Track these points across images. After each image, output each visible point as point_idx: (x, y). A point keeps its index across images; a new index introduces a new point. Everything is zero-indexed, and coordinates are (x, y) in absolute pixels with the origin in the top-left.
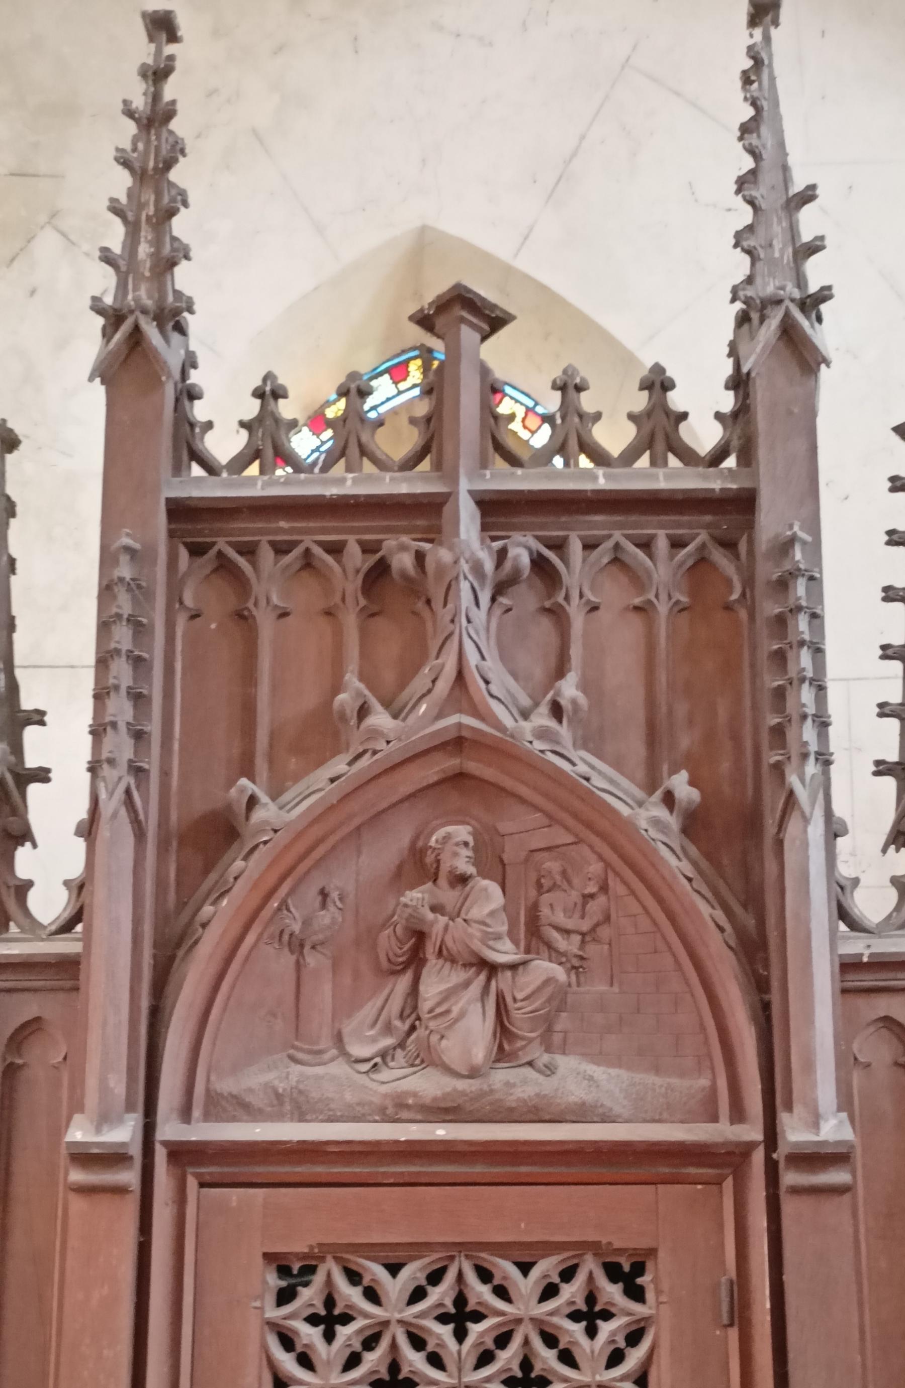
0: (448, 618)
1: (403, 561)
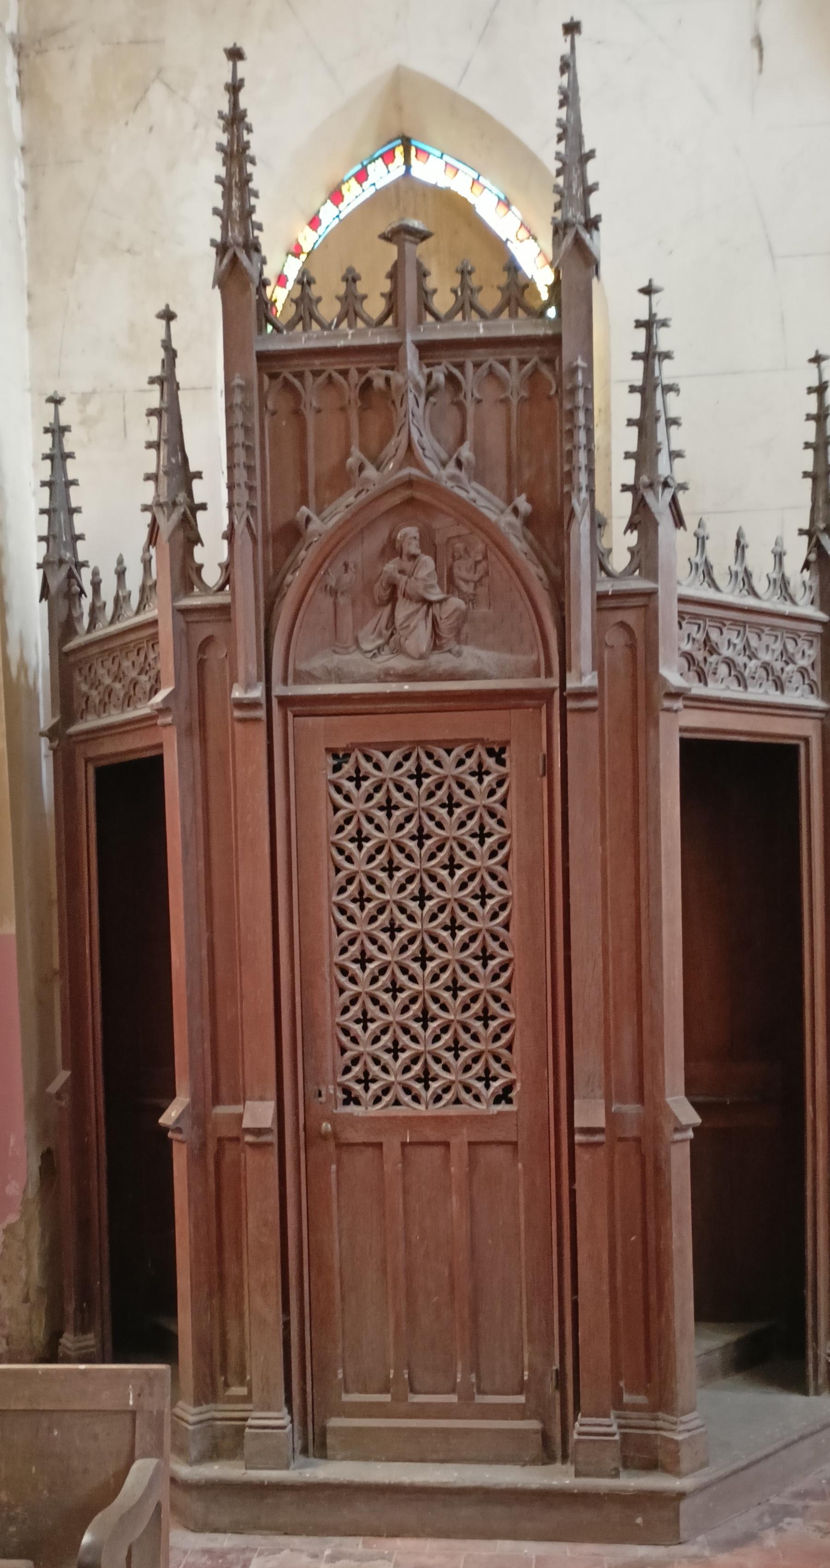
0: (403, 414)
1: (379, 383)
